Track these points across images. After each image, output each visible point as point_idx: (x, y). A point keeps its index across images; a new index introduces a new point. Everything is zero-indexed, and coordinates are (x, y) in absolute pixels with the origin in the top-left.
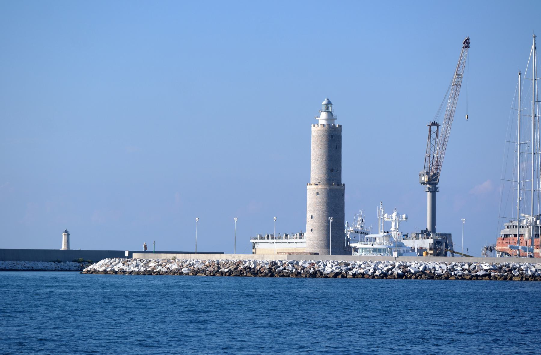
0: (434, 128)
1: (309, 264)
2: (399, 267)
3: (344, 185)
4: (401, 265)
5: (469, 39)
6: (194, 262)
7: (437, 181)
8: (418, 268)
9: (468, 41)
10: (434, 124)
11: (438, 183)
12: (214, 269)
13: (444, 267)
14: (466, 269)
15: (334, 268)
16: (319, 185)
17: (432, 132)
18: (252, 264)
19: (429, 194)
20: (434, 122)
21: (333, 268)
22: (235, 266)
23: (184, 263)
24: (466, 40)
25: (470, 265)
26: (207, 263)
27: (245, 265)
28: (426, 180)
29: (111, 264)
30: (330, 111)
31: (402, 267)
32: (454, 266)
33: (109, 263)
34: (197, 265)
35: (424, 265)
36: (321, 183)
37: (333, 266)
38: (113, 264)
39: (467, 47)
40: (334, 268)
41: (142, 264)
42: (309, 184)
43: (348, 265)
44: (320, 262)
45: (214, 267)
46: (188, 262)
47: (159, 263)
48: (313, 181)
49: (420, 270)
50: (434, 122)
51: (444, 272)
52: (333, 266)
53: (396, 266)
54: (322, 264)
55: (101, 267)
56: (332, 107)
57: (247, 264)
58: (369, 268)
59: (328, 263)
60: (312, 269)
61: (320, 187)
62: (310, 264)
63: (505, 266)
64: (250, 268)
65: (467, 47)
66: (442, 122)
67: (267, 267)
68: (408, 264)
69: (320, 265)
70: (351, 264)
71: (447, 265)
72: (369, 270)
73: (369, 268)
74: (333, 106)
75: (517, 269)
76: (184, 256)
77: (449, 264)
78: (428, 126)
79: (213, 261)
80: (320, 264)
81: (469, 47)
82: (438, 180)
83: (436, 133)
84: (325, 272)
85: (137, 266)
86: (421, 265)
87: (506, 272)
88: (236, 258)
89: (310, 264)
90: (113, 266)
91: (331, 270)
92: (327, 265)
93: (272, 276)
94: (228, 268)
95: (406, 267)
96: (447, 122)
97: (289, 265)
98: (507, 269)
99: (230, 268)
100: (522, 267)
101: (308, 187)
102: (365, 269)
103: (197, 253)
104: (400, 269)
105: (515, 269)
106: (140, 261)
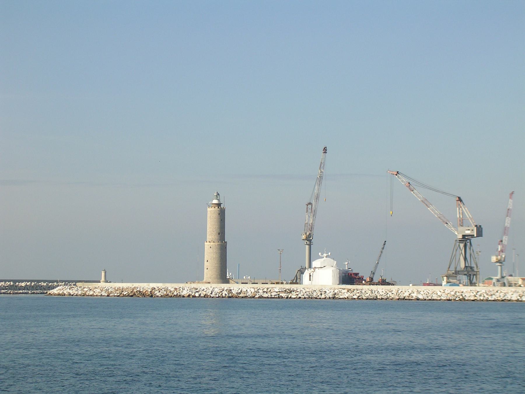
0: (310, 206)
1: (174, 289)
2: (226, 290)
3: (226, 242)
4: (228, 289)
5: (326, 147)
6: (109, 288)
7: (311, 238)
8: (238, 291)
9: (326, 148)
10: (310, 204)
11: (312, 240)
12: (120, 292)
13: (253, 290)
14: (265, 292)
15: (188, 291)
16: (212, 242)
17: (308, 209)
18: (141, 289)
19: (307, 247)
20: (310, 203)
21: (188, 291)
22: (132, 290)
23: (104, 288)
24: (325, 148)
25: (267, 289)
26: (116, 288)
27: (137, 290)
28: (305, 238)
29: (63, 289)
30: (218, 199)
31: (228, 290)
32: (258, 290)
33: (62, 289)
34: (111, 289)
35: (241, 289)
36: (212, 241)
37: (188, 290)
38: (64, 289)
39: (325, 152)
40: (188, 291)
41: (80, 289)
42: (206, 242)
43: (197, 289)
44: (180, 287)
45: (120, 291)
46: (106, 288)
47: (90, 289)
48: (208, 240)
49: (238, 292)
50: (310, 203)
51: (252, 293)
52: (188, 290)
53: (225, 290)
54: (182, 289)
55: (57, 291)
56: (219, 197)
57: (138, 289)
58: (209, 291)
59: (185, 288)
60: (176, 292)
61: (212, 243)
62: (175, 288)
63: (288, 289)
64: (140, 292)
65: (325, 152)
66: (313, 203)
67: (150, 291)
68: (232, 289)
69: (180, 290)
70: (198, 289)
71: (254, 289)
72: (209, 292)
73: (209, 291)
74: (220, 196)
75: (295, 291)
76: (283, 286)
77: (256, 289)
78: (306, 205)
79: (120, 288)
80: (180, 289)
81: (326, 153)
82: (312, 237)
83: (311, 209)
84: (183, 294)
85: (78, 290)
86: (239, 289)
87: (288, 293)
88: (171, 287)
89: (175, 288)
90: (64, 290)
91: (186, 292)
92: (184, 289)
93: (152, 296)
94: (128, 291)
95: (231, 290)
96: (316, 201)
97: (163, 289)
98: (289, 292)
99: (129, 291)
100: (297, 290)
101: (206, 243)
102: (206, 292)
103: (281, 284)
104: (227, 291)
105: (294, 291)
106: (80, 287)
